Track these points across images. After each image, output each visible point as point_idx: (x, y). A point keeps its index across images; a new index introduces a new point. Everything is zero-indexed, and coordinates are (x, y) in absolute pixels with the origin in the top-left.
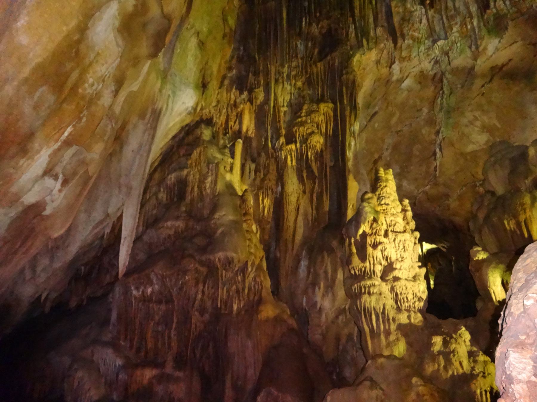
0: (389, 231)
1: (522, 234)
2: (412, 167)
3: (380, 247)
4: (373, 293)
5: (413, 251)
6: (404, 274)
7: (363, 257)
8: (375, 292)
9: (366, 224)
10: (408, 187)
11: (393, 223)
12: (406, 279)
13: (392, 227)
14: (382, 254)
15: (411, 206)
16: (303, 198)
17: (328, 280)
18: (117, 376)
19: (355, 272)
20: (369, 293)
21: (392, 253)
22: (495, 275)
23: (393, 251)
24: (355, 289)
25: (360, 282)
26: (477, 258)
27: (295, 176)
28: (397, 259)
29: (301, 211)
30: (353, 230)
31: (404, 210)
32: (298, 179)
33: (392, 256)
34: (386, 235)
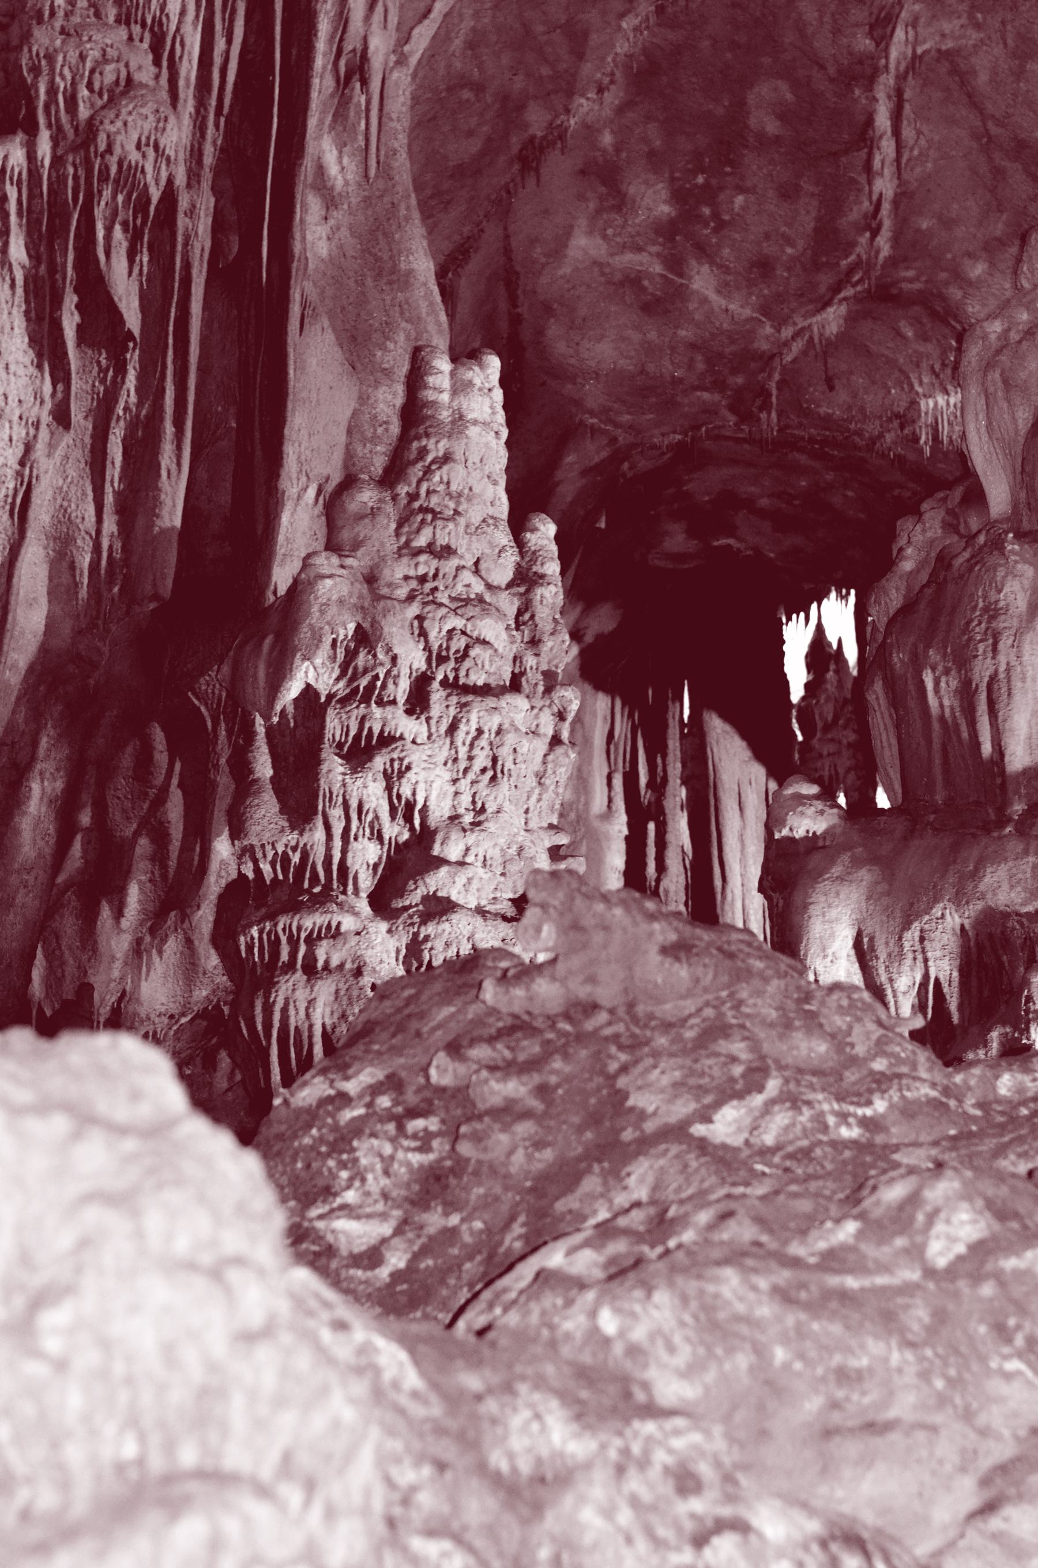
0: (436, 685)
1: (976, 745)
2: (739, 200)
3: (379, 762)
4: (326, 967)
5: (540, 777)
6: (475, 884)
7: (301, 802)
8: (335, 962)
9: (321, 657)
10: (717, 301)
11: (459, 643)
12: (481, 911)
13: (452, 664)
14: (389, 788)
15: (564, 558)
16: (51, 447)
17: (164, 867)
18: (458, 1127)
19: (258, 871)
20: (310, 970)
21: (432, 785)
22: (833, 913)
23: (443, 776)
24: (250, 948)
25: (273, 917)
26: (785, 832)
27: (19, 322)
28: (454, 818)
29: (41, 515)
30: (261, 674)
31: (526, 578)
32: (34, 341)
33: (432, 804)
34: (418, 702)
